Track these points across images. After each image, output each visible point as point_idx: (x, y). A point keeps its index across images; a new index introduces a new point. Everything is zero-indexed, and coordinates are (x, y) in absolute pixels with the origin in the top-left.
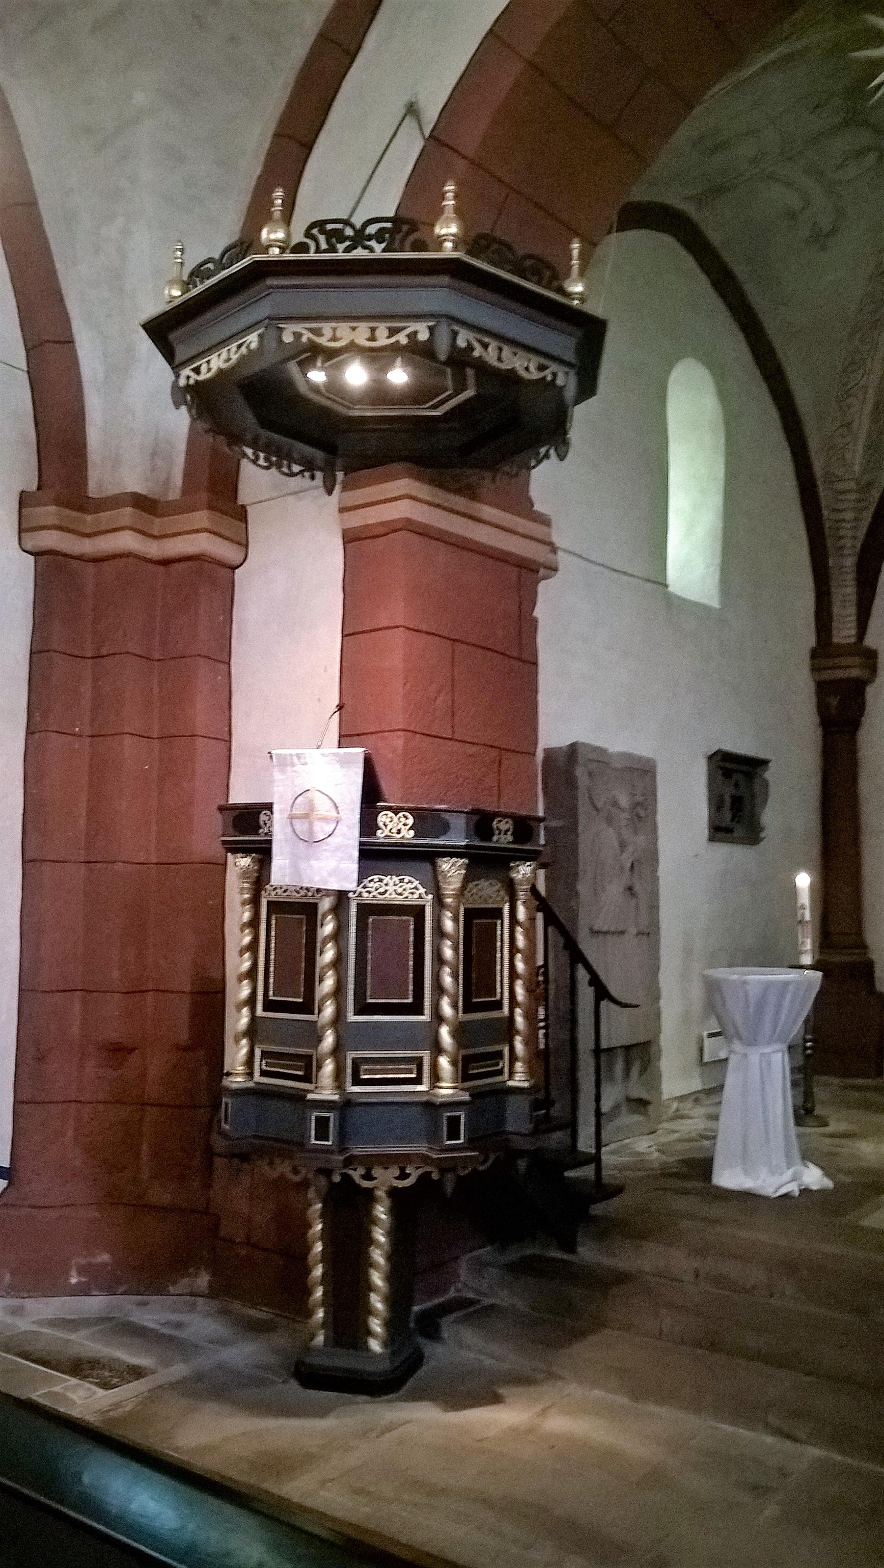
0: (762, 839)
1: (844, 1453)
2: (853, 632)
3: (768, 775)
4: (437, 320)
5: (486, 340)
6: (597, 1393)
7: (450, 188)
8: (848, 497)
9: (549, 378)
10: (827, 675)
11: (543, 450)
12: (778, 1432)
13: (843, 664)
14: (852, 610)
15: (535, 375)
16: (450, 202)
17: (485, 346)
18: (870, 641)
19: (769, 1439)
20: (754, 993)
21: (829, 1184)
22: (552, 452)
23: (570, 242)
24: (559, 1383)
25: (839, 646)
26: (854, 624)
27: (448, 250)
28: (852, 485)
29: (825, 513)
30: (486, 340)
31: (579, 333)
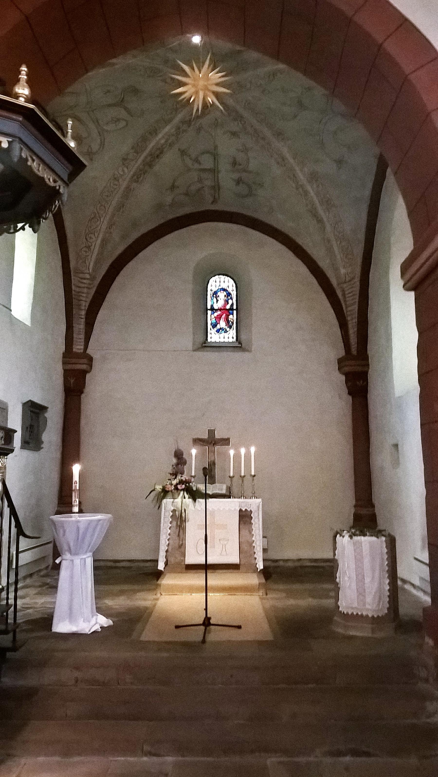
0: (43, 448)
1: (183, 756)
2: (82, 347)
3: (46, 415)
4: (14, 139)
5: (34, 158)
6: (41, 759)
7: (24, 69)
8: (85, 281)
9: (58, 188)
10: (69, 367)
11: (20, 225)
12: (150, 754)
13: (80, 362)
14: (82, 336)
15: (52, 184)
16: (23, 77)
17: (33, 160)
18: (89, 351)
19: (145, 759)
20: (82, 527)
21: (111, 622)
22: (27, 227)
23: (67, 120)
24: (16, 759)
25: (77, 353)
26: (83, 344)
27: (21, 101)
28: (88, 276)
29: (73, 287)
30: (34, 158)
31: (71, 168)
